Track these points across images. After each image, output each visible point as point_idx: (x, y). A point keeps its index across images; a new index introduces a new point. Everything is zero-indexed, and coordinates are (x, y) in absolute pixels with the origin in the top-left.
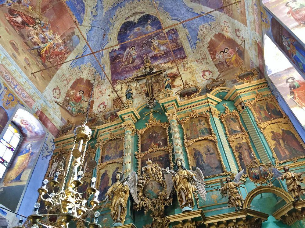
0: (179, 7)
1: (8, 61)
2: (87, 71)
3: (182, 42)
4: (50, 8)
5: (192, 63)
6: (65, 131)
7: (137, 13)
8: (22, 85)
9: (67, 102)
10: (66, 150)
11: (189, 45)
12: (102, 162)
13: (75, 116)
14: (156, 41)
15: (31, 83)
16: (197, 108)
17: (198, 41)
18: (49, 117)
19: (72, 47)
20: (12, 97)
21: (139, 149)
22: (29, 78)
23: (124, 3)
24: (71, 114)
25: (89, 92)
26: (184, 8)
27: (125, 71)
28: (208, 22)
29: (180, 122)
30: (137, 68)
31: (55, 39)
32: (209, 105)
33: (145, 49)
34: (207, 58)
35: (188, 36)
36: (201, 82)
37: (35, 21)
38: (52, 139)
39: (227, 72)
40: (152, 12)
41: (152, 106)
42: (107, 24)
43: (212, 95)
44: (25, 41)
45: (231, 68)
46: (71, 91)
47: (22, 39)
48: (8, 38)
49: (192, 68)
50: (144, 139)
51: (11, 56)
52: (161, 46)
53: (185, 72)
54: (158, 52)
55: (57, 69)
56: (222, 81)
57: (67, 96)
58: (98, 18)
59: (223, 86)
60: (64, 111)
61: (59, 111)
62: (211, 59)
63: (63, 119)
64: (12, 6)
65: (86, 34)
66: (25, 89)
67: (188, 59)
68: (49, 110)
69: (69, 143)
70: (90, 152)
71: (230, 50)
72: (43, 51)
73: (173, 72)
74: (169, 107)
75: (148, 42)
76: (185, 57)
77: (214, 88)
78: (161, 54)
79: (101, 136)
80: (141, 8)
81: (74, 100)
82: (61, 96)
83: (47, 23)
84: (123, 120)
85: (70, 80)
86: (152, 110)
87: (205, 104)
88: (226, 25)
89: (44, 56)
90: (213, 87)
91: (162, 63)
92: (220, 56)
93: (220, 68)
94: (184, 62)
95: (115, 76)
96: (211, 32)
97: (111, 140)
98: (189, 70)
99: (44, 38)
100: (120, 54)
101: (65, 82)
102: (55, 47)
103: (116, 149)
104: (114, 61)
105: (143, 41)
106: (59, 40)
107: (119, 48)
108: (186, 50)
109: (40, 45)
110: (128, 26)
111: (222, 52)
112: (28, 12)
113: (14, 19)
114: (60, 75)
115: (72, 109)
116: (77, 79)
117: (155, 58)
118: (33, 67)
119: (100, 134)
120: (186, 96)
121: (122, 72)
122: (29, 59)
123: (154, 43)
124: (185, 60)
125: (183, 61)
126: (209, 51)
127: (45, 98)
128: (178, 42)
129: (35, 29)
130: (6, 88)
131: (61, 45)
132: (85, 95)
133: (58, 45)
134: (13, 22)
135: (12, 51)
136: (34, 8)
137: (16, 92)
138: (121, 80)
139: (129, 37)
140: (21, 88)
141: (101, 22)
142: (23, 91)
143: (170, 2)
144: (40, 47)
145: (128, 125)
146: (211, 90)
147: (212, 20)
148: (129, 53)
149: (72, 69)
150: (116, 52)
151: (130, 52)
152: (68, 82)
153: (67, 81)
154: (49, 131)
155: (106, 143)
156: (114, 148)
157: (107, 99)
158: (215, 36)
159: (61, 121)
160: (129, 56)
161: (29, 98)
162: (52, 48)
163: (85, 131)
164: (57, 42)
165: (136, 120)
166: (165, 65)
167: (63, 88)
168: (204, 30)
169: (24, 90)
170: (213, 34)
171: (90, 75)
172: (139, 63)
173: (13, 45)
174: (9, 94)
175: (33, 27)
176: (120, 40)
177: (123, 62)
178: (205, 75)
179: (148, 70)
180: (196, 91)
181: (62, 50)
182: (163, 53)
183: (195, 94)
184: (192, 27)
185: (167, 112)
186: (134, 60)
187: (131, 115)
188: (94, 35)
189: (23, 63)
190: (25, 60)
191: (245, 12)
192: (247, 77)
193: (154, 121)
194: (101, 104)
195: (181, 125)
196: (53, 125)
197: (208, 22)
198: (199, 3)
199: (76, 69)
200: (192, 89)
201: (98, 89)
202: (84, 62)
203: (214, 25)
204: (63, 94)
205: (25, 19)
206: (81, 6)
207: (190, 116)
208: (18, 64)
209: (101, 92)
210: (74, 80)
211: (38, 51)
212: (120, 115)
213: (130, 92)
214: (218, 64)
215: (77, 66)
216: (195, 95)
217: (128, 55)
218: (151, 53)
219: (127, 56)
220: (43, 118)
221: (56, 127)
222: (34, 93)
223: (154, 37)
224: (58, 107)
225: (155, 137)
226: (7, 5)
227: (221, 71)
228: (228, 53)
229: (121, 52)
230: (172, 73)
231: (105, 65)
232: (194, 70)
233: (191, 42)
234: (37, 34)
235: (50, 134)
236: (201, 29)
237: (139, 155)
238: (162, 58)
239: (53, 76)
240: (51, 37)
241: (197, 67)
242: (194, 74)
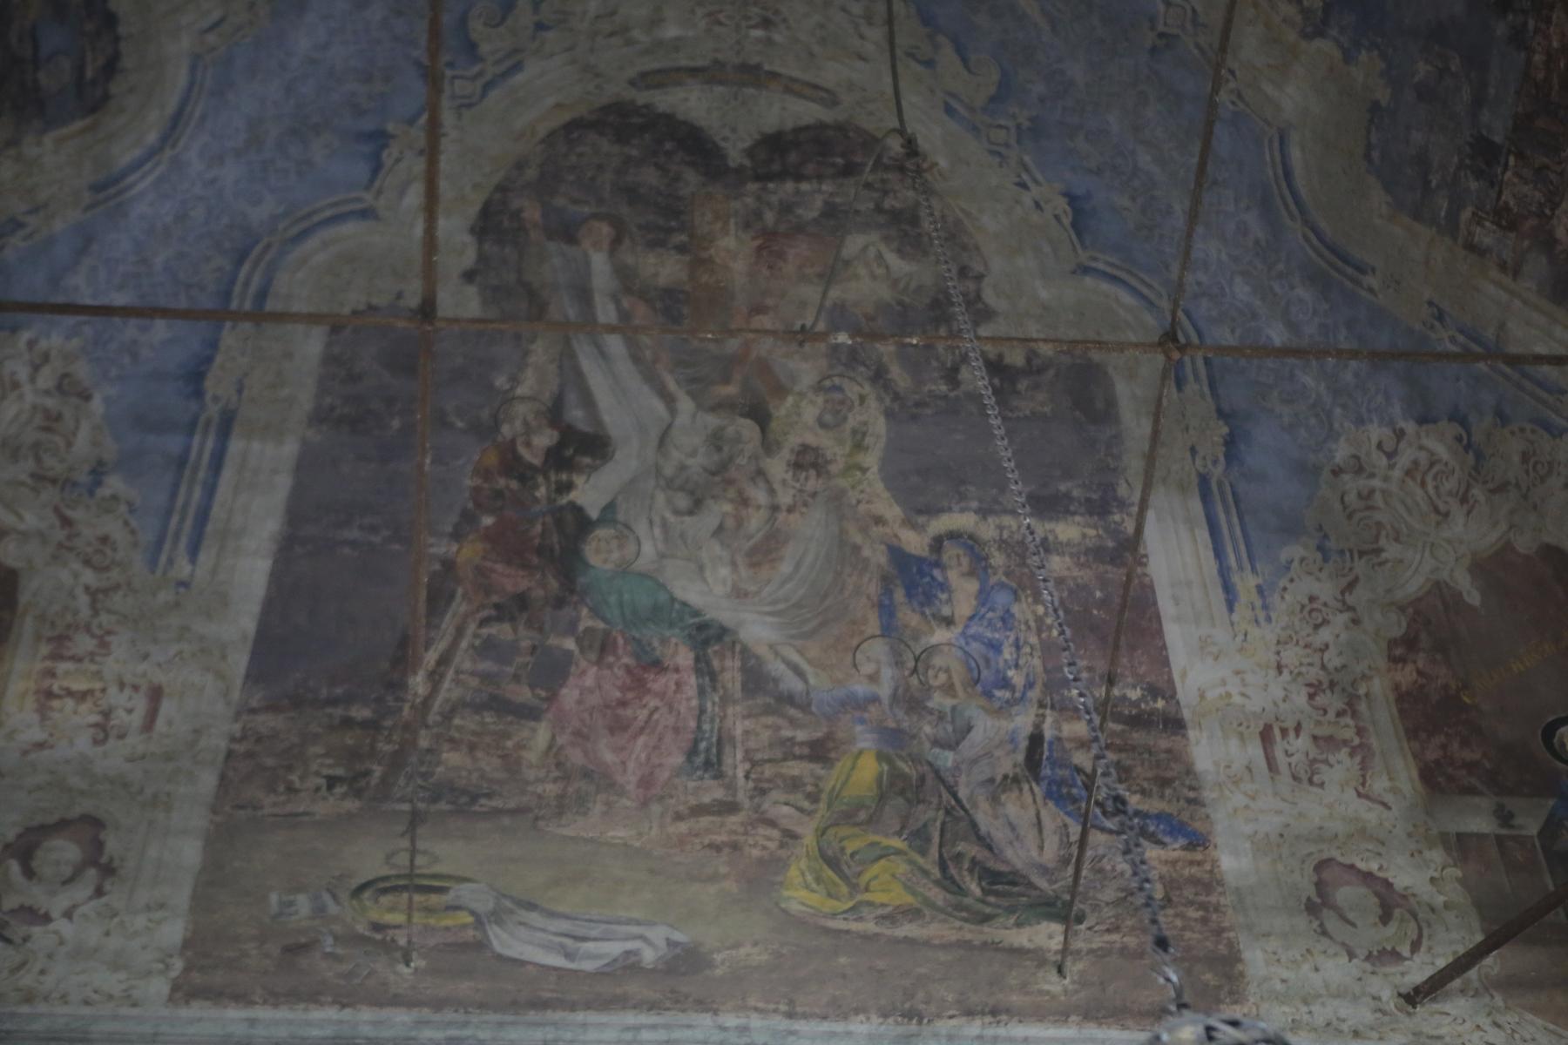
35: (21, 233)
88: (115, 697)
168: (30, 398)
191: (313, 997)
203: (104, 540)
236: (46, 358)
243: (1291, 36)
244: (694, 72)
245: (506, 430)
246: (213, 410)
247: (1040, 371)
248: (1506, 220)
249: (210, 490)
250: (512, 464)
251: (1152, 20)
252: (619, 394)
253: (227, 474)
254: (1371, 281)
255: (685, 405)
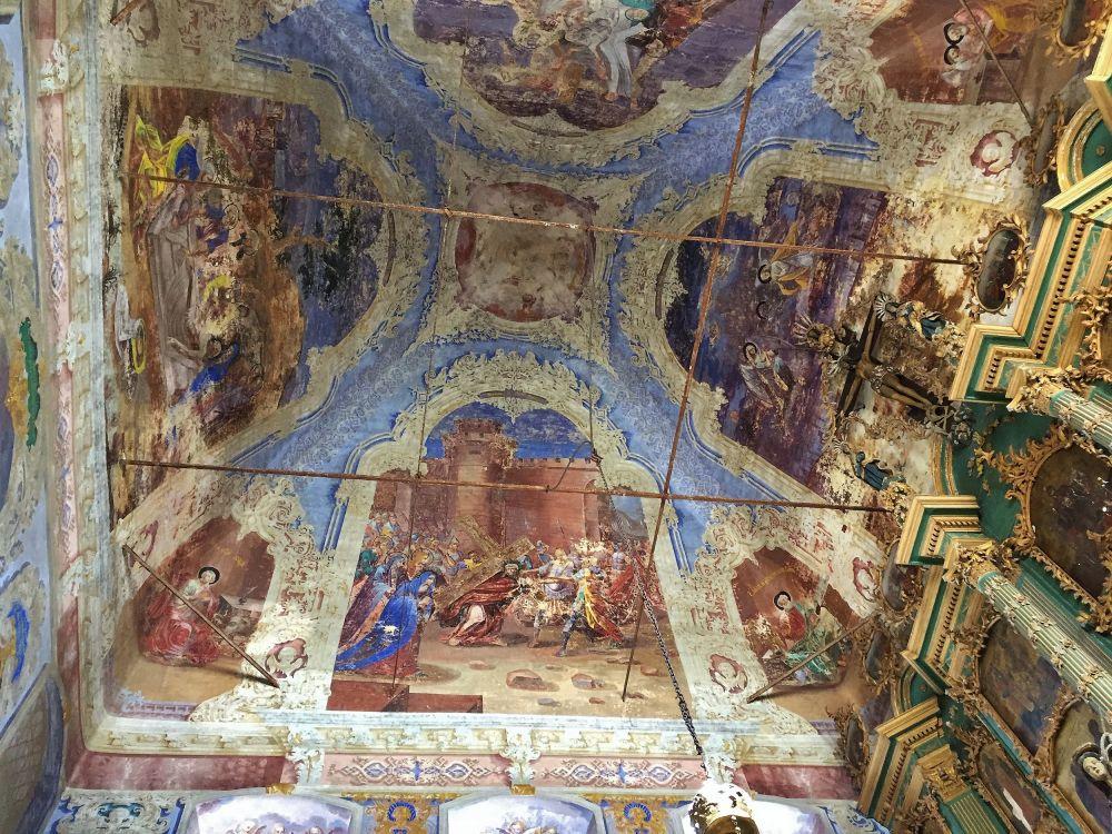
0: (717, 132)
1: (545, 733)
2: (730, 533)
3: (826, 181)
4: (503, 514)
5: (918, 184)
6: (857, 756)
7: (662, 274)
8: (631, 754)
9: (777, 668)
10: (916, 810)
11: (850, 160)
12: (1033, 751)
13: (842, 680)
14: (774, 265)
15: (643, 723)
16: (1079, 274)
17: (857, 121)
18: (779, 759)
19: (635, 525)
20: (639, 810)
21: (1080, 598)
22: (629, 715)
23: (614, 295)
24: (825, 685)
25: (796, 575)
26: (727, 118)
27: (801, 426)
28: (812, 58)
29: (1085, 376)
30: (813, 382)
31: (585, 559)
32: (1098, 223)
33: (778, 315)
34: (935, 119)
36: (1002, 190)
37: (507, 576)
38: (854, 813)
39: (1034, 74)
40: (685, 225)
41: (963, 426)
42: (639, 378)
43: (1073, 182)
44: (535, 642)
45: (1031, 48)
46: (753, 628)
47: (523, 648)
48: (497, 682)
49: (936, 196)
50: (1057, 545)
51: (542, 713)
52: (796, 259)
53: (934, 226)
54: (811, 280)
55: (663, 617)
56: (1049, 113)
57: (760, 654)
58: (611, 398)
59: (1067, 123)
60: (796, 699)
61: (786, 713)
62: (946, 108)
63: (819, 724)
64: (436, 605)
65: (629, 459)
66: (648, 753)
67: (894, 189)
68: (758, 741)
69: (901, 778)
70: (977, 748)
71: (961, 18)
72: (591, 615)
73: (905, 272)
74: (998, 377)
75: (759, 291)
76: (882, 194)
77: (1053, 160)
78: (822, 275)
79: (947, 668)
80: (654, 253)
81: (787, 641)
82: (748, 672)
83: (532, 547)
84: (939, 561)
85: (719, 604)
86: (977, 438)
87: (1086, 234)
89: (605, 624)
90: (1047, 160)
91: (852, 290)
92: (959, 66)
93: (1004, 89)
94: (897, 212)
95: (796, 466)
96: (854, 62)
97: (982, 652)
98: (935, 210)
99: (562, 585)
100: (742, 402)
101: (717, 624)
102: (605, 575)
103: (1026, 668)
104: (751, 436)
105: (748, 307)
106: (592, 550)
107: (724, 394)
108: (862, 179)
109: (569, 612)
110: (679, 324)
111: (951, 51)
112: (475, 577)
113: (466, 626)
114: (684, 621)
115: (813, 669)
116: (733, 581)
117: (821, 301)
118: (610, 679)
119: (939, 666)
120: (1005, 286)
121: (798, 434)
122: (584, 671)
123: (773, 276)
124: (891, 203)
125: (891, 215)
126: (916, 98)
127: (716, 721)
128: (819, 196)
129: (524, 592)
130: (604, 803)
131: (610, 556)
132: (796, 598)
133: (604, 563)
134: (471, 634)
135: (531, 699)
136: (478, 553)
137: (635, 787)
138: (821, 456)
139: (712, 340)
140: (635, 761)
141: (627, 392)
142: (649, 765)
143: (687, 153)
144: (576, 617)
145: (962, 560)
146: (1053, 175)
147: (811, 43)
148: (756, 373)
149: (695, 574)
150: (730, 409)
151: (755, 369)
152: (723, 615)
153: (716, 615)
154: (819, 797)
155: (981, 680)
156: (1016, 669)
157: (853, 544)
158: (876, 51)
159: (820, 732)
160: (766, 381)
161: (679, 766)
162: (599, 585)
163: (712, 808)
164: (594, 560)
165: (975, 518)
166: (866, 284)
167: (729, 643)
169: (647, 758)
170: (864, 57)
171: (749, 536)
172: (805, 362)
173: (520, 682)
174: (626, 811)
175: (516, 594)
176: (706, 373)
177: (773, 410)
178: (992, 162)
179: (841, 351)
180: (1012, 239)
181: (624, 561)
182: (821, 265)
183: (1020, 252)
184: (801, 119)
185: (1010, 400)
186: (786, 374)
187: (938, 523)
188: (647, 439)
189: (580, 698)
190: (578, 685)
192: (1089, 11)
193: (1019, 465)
194: (856, 573)
195: (1099, 382)
196: (812, 767)
197: (812, 58)
198: (736, 62)
199: (702, 562)
200: (992, 250)
201: (802, 545)
202: (701, 522)
203: (832, 41)
204: (747, 658)
205: (484, 597)
206: (552, 423)
207: (1088, 323)
208: (573, 711)
209: (817, 545)
210: (730, 591)
211: (579, 630)
212: (911, 559)
213: (865, 462)
214: (983, 89)
215: (697, 551)
216: (1024, 251)
217: (759, 378)
218: (798, 305)
219: (762, 384)
220: (767, 779)
221: (826, 767)
222: (677, 739)
223: (756, 263)
224: (770, 705)
225: (1080, 506)
226: (427, 616)
227: (1014, 96)
228: (967, 33)
229: (739, 394)
230: (906, 278)
231: (747, 468)
232: (948, 192)
233: (845, 147)
234: (539, 596)
235: (831, 803)
237: (1103, 616)
238: (834, 279)
239: (672, 643)
240: (571, 564)
241: (945, 175)
242: (959, 198)
243: (349, 158)
244: (563, 135)
245: (666, 50)
246: (773, 68)
247: (444, 38)
248: (271, 121)
249: (786, 48)
250: (667, 41)
251: (394, 146)
252: (618, 54)
253: (776, 53)
254: (312, 71)
255: (593, 48)
